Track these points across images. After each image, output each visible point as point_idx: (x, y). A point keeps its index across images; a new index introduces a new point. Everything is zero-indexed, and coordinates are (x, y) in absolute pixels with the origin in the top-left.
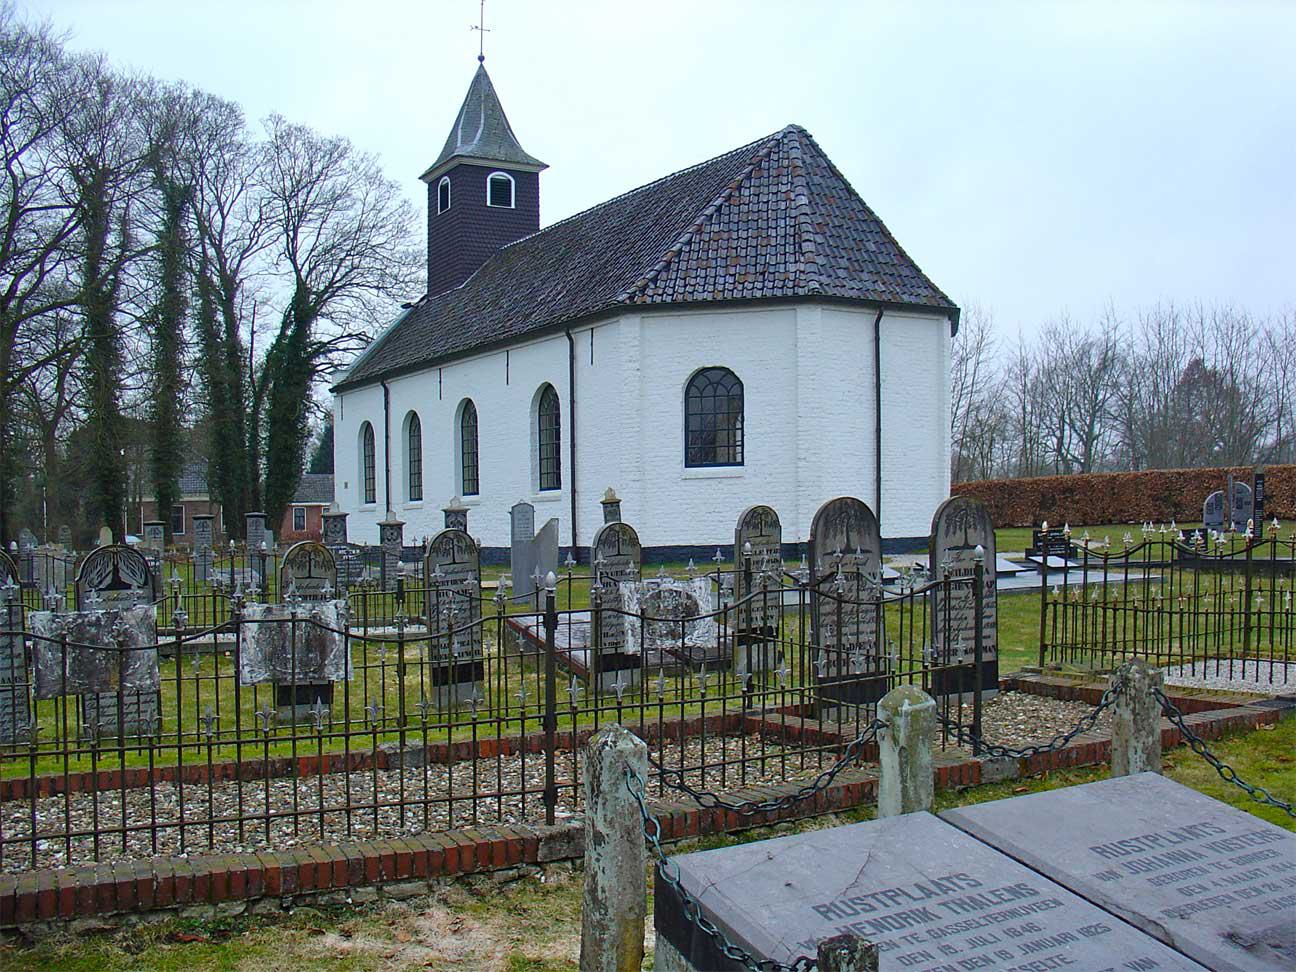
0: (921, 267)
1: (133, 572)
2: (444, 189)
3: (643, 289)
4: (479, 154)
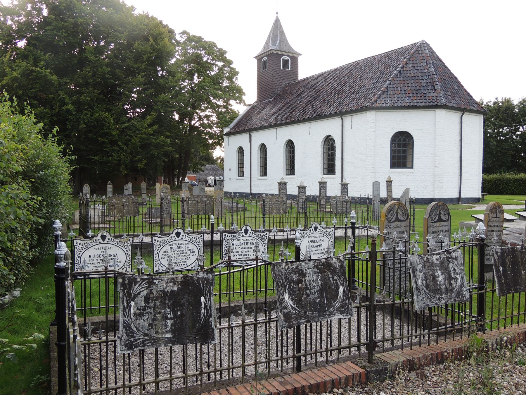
0: (472, 96)
1: (445, 214)
2: (265, 62)
3: (376, 101)
4: (279, 49)
